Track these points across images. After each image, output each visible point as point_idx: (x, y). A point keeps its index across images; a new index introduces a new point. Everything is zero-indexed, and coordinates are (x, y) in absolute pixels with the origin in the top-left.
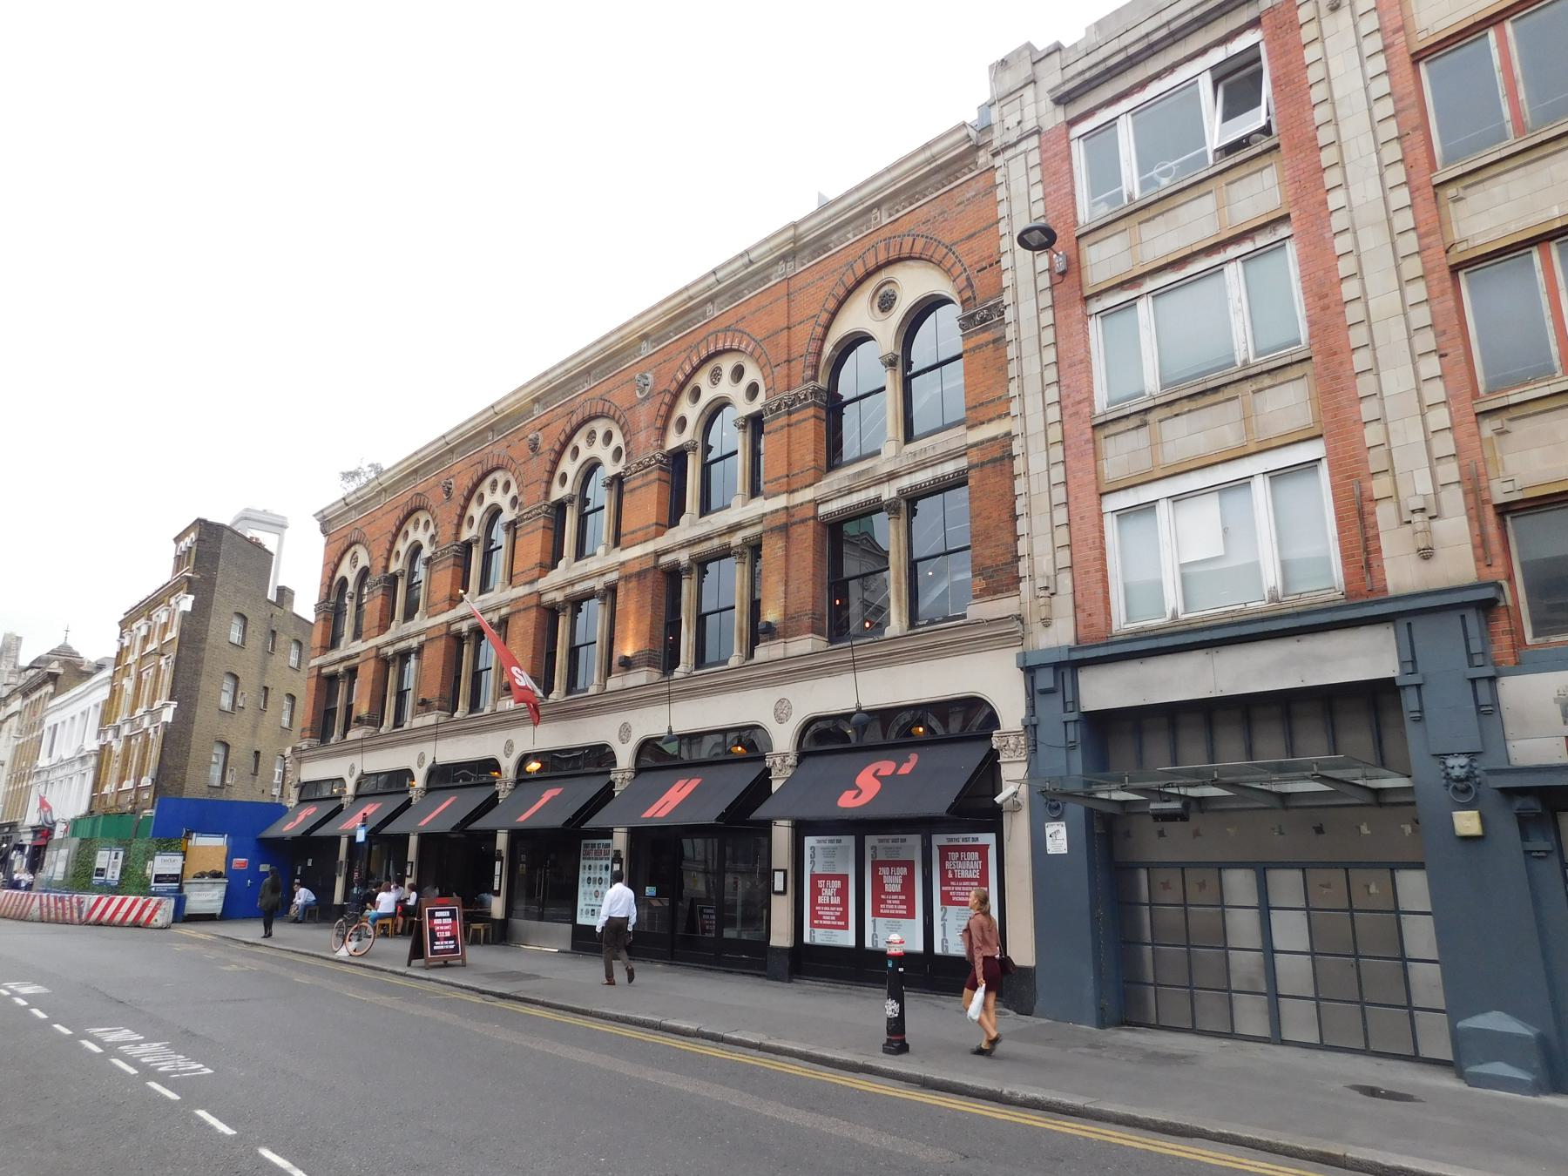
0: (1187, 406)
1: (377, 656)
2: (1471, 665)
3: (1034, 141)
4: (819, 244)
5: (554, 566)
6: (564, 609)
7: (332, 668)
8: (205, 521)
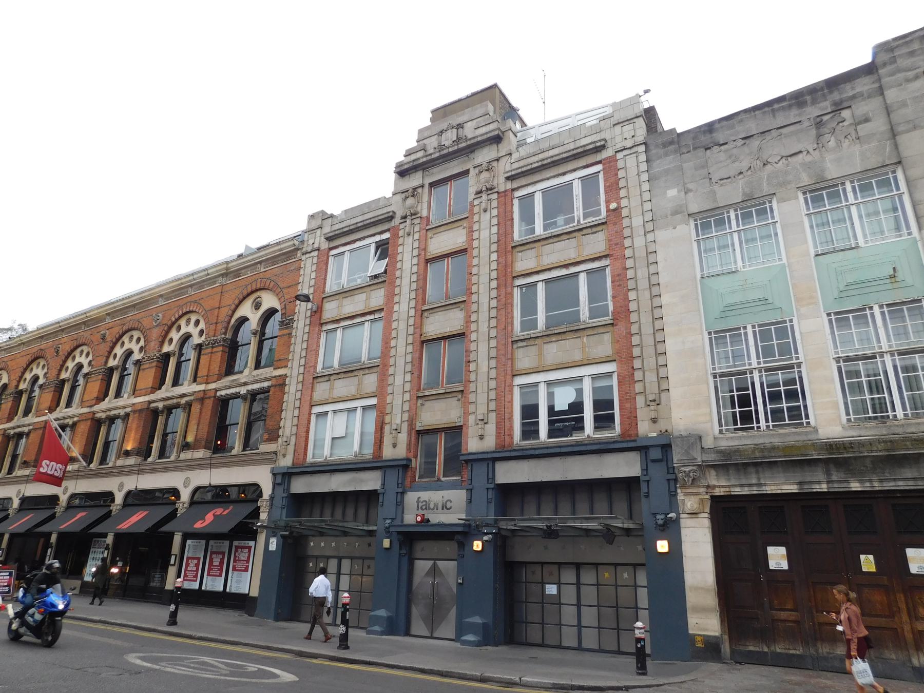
2: (668, 473)
3: (316, 253)
4: (237, 273)
5: (160, 388)
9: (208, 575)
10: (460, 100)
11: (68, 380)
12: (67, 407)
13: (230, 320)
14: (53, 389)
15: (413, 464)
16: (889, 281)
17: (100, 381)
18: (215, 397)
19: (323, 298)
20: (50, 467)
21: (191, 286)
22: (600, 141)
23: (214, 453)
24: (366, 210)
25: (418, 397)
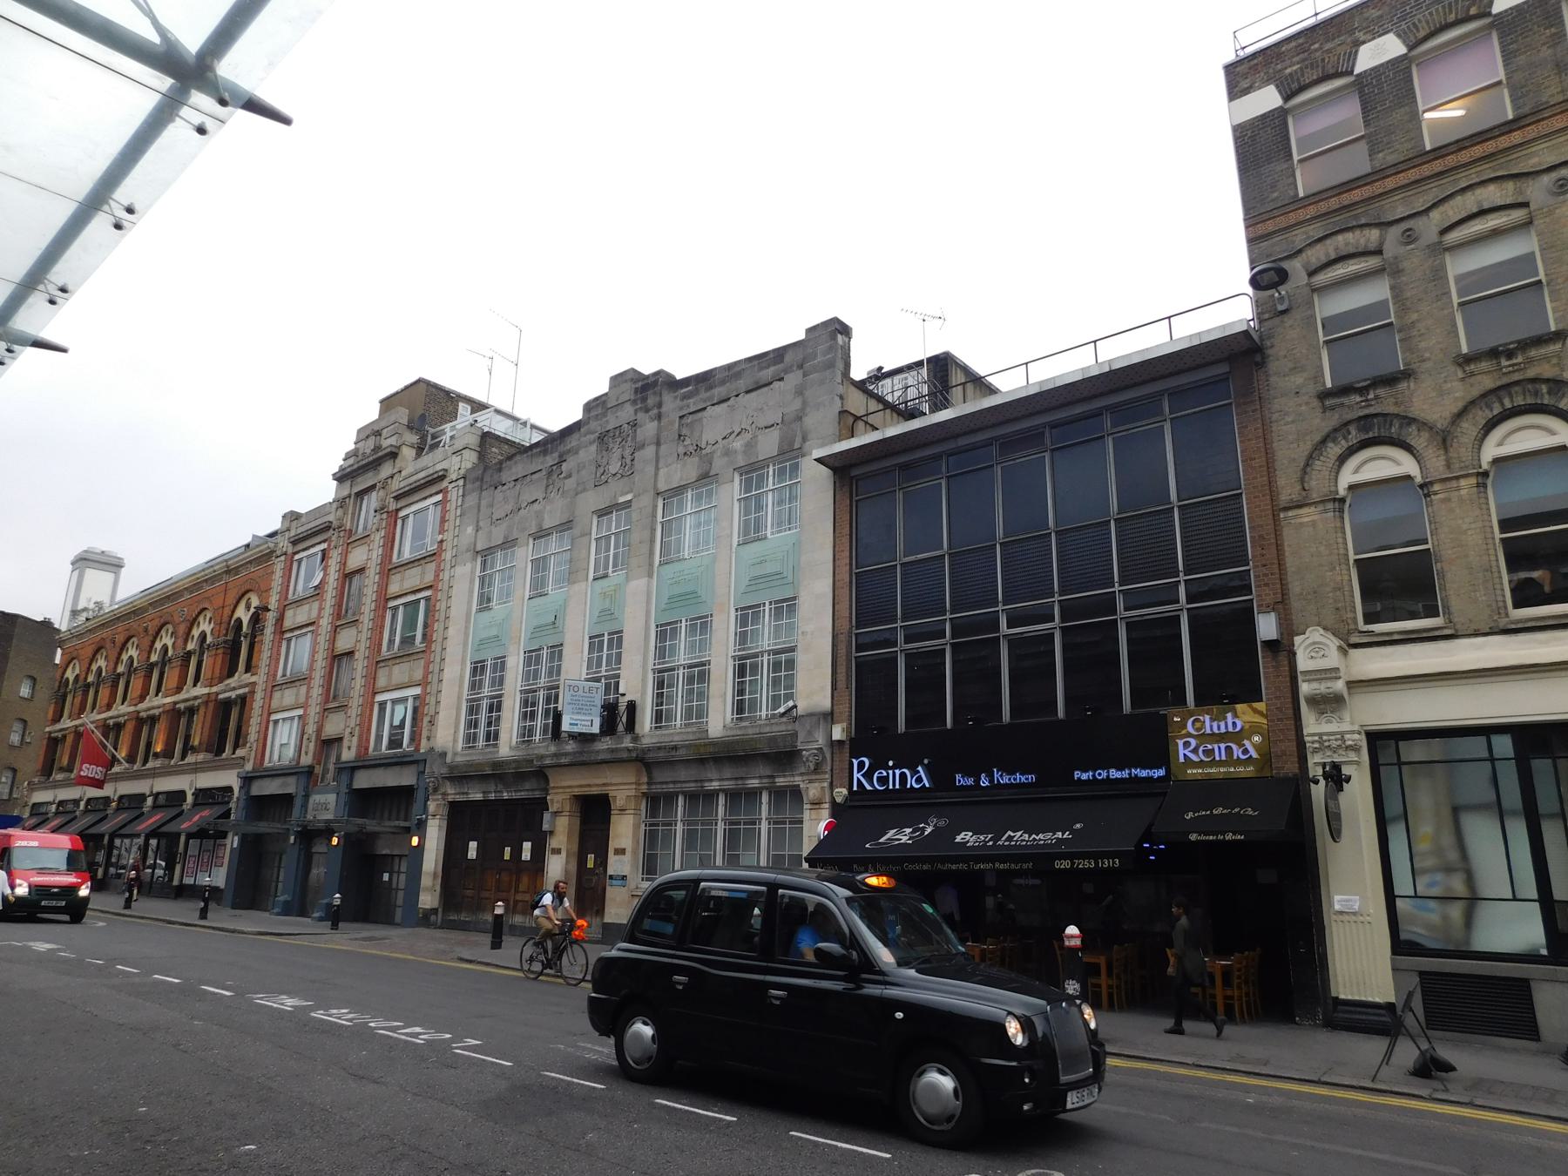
0: (288, 685)
1: (75, 731)
4: (236, 570)
5: (59, 721)
6: (236, 704)
7: (56, 734)
8: (428, 384)
9: (201, 871)
10: (397, 393)
11: (123, 674)
12: (246, 672)
13: (230, 621)
14: (110, 684)
15: (316, 771)
16: (551, 627)
17: (179, 668)
18: (216, 700)
19: (389, 570)
20: (90, 772)
21: (206, 581)
22: (441, 470)
23: (216, 755)
24: (318, 516)
25: (325, 710)
